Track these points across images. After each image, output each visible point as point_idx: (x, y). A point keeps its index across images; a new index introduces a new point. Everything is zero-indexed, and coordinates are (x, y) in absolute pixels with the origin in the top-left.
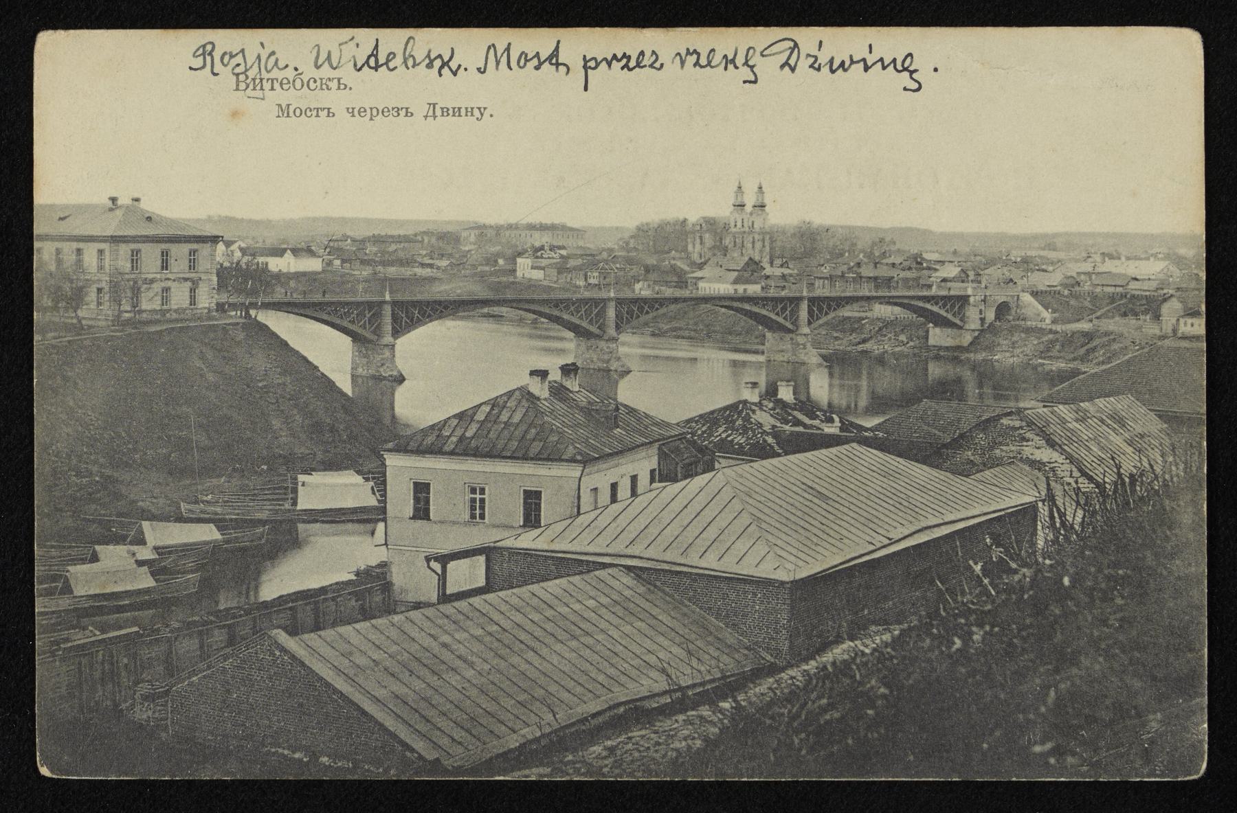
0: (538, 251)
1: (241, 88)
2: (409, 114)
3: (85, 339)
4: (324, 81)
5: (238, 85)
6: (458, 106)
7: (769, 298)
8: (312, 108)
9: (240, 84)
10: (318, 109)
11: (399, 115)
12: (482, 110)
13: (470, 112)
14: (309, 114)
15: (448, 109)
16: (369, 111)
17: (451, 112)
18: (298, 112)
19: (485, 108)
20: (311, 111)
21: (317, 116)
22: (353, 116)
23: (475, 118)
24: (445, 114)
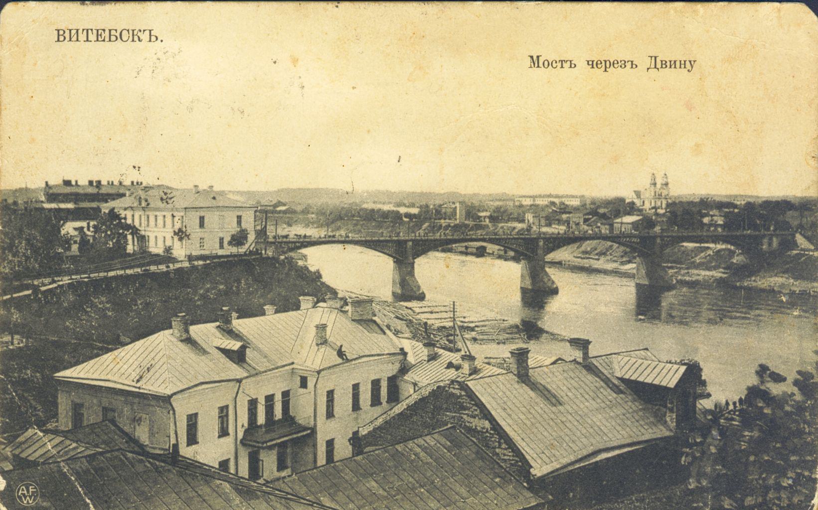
0: (565, 213)
1: (60, 40)
2: (572, 65)
3: (50, 284)
4: (135, 33)
5: (150, 38)
6: (673, 59)
7: (470, 327)
8: (626, 61)
9: (60, 37)
10: (562, 61)
11: (625, 66)
12: (692, 63)
13: (683, 64)
14: (554, 65)
15: (666, 62)
16: (603, 63)
17: (668, 64)
18: (546, 63)
19: (694, 61)
20: (556, 62)
21: (562, 67)
22: (593, 67)
23: (686, 70)
24: (664, 66)
